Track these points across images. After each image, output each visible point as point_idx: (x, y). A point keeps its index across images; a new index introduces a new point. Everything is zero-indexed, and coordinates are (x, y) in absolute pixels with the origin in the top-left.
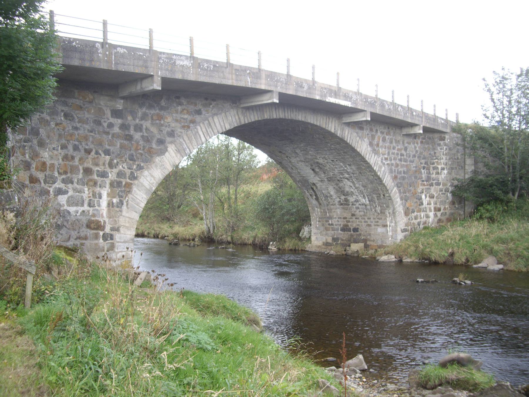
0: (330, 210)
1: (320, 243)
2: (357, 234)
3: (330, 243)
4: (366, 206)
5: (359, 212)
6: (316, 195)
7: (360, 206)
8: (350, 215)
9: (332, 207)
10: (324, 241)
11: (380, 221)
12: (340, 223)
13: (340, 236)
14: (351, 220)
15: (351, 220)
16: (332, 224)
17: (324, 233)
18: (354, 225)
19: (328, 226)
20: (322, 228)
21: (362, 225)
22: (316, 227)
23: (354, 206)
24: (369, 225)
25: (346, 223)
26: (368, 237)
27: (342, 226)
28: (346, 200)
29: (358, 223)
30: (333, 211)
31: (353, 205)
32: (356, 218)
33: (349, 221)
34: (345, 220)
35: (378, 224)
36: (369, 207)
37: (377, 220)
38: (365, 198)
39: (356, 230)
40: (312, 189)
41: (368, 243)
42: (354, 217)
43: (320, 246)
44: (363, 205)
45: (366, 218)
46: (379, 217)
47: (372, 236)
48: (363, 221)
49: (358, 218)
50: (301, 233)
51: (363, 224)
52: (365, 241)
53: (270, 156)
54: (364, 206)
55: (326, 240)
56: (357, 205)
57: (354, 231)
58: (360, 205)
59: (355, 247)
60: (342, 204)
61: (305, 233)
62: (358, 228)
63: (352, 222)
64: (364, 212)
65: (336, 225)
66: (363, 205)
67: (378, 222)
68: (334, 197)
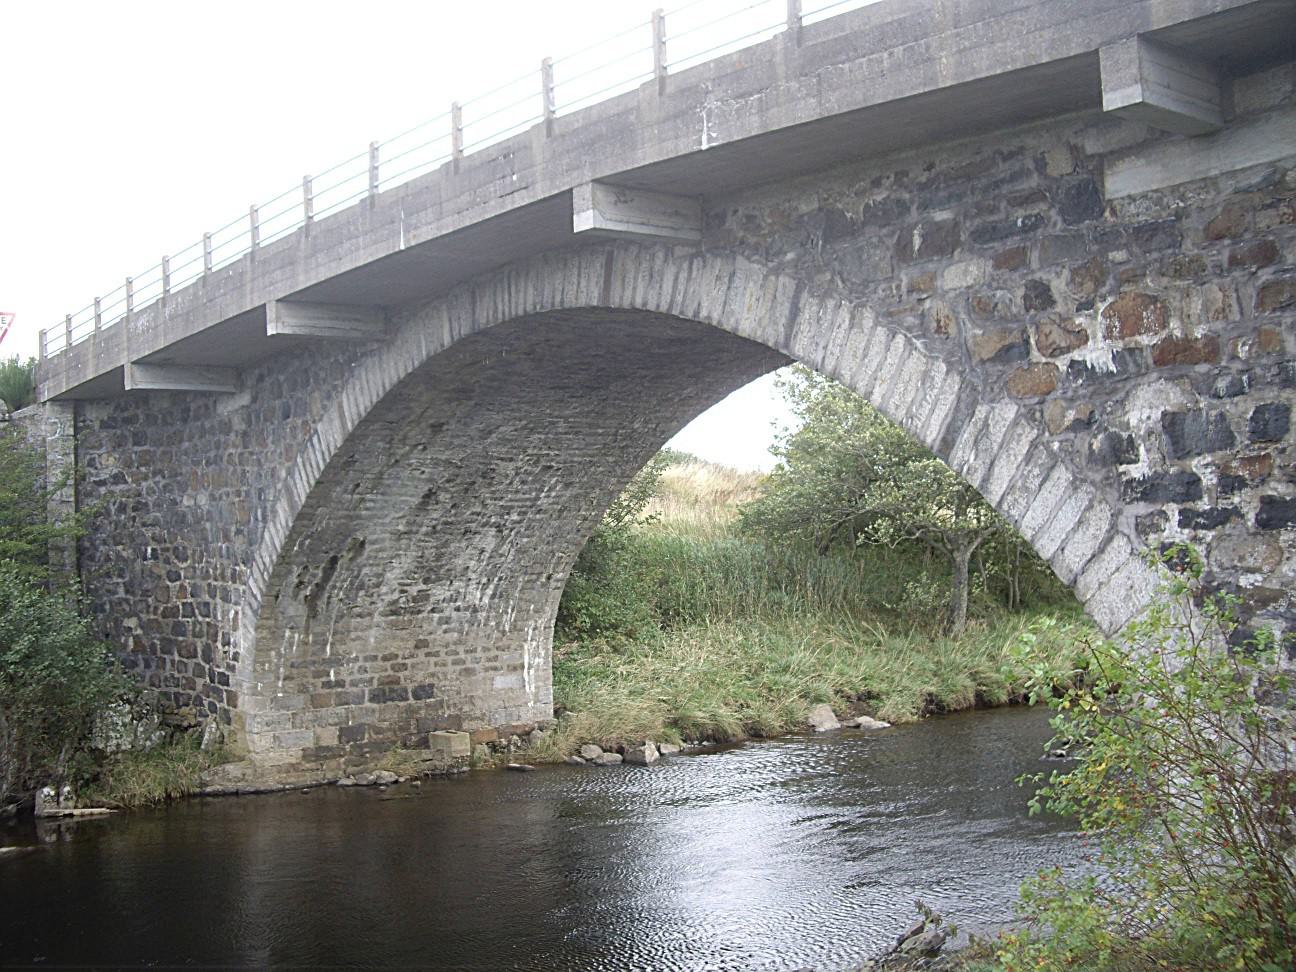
0: (341, 635)
1: (292, 755)
2: (428, 706)
3: (328, 748)
5: (445, 632)
7: (454, 614)
8: (411, 644)
9: (354, 622)
10: (310, 744)
11: (505, 656)
12: (367, 676)
16: (340, 683)
17: (309, 716)
18: (420, 677)
20: (299, 701)
21: (445, 674)
22: (274, 700)
24: (469, 672)
26: (466, 708)
27: (375, 682)
28: (423, 596)
29: (432, 669)
32: (428, 655)
34: (388, 664)
36: (482, 615)
39: (424, 691)
42: (421, 653)
44: (466, 609)
47: (478, 703)
49: (437, 654)
51: (450, 668)
55: (318, 738)
57: (417, 697)
58: (458, 609)
60: (394, 613)
62: (432, 686)
64: (461, 632)
65: (354, 684)
67: (496, 658)
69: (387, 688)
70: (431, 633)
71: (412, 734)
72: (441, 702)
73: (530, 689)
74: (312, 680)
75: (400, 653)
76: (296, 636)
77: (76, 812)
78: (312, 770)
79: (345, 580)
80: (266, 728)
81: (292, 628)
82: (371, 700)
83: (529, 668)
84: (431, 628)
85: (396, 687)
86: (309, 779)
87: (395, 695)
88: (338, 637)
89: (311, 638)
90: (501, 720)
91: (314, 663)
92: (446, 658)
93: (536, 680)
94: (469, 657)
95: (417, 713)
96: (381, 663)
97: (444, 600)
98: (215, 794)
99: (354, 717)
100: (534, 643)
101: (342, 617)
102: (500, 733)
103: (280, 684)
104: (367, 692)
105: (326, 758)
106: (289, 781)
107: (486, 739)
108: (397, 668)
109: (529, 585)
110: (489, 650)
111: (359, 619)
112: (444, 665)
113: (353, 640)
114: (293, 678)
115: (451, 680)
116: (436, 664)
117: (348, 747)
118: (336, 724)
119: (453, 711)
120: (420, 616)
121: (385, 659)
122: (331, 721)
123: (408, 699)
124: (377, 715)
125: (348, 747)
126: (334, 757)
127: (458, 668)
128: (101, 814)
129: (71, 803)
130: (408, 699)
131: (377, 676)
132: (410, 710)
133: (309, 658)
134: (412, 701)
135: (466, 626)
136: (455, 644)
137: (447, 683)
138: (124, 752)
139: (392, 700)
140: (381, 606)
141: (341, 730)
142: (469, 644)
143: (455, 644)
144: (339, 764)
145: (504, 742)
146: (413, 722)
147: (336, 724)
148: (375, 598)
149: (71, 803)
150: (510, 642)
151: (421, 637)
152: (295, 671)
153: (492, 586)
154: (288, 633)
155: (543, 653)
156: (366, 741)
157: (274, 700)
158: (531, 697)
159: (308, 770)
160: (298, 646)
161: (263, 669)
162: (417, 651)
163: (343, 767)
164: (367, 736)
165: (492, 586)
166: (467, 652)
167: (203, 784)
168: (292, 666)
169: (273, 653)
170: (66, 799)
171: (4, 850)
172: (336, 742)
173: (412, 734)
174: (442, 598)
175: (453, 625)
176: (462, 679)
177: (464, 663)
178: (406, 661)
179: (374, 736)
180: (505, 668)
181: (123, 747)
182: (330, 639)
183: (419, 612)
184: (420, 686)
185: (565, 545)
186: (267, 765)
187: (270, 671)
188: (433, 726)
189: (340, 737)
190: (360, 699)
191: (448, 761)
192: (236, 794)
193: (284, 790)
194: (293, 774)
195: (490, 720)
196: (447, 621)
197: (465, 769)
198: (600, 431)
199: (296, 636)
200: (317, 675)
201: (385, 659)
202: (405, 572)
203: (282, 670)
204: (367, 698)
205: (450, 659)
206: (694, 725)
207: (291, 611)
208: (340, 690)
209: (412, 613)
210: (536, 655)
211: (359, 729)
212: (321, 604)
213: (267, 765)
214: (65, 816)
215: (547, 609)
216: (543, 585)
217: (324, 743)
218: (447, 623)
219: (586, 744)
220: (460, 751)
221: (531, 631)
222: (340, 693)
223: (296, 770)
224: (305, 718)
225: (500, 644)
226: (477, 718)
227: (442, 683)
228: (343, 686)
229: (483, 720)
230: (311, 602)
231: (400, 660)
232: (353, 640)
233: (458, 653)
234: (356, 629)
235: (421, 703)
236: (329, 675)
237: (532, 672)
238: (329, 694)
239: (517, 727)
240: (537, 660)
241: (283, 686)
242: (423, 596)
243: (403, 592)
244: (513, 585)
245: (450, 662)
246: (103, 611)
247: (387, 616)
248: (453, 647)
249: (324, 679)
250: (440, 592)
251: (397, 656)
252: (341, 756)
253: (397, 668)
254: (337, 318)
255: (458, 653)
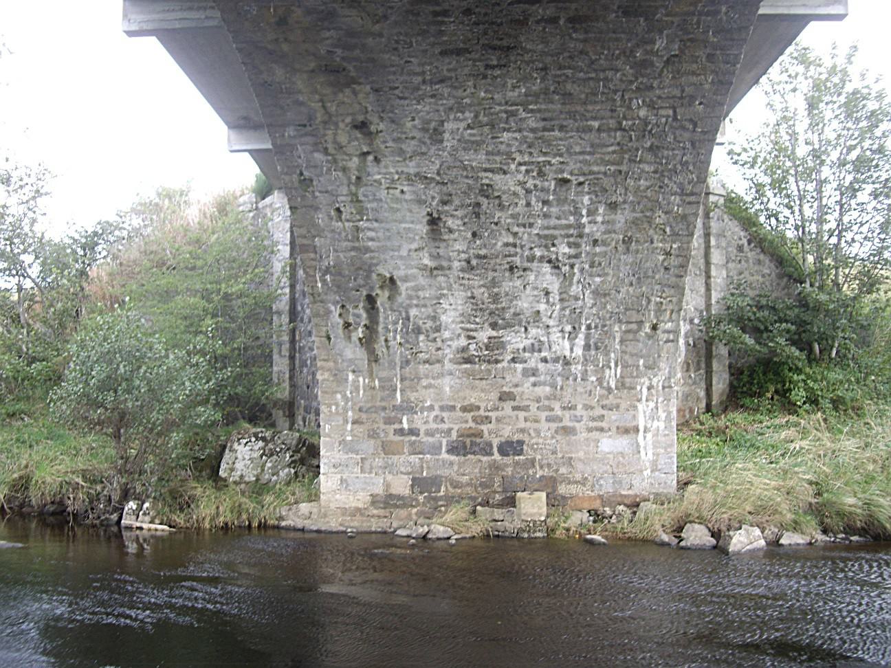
0: (412, 382)
1: (360, 499)
2: (517, 463)
3: (399, 497)
4: (567, 363)
5: (534, 385)
6: (371, 329)
7: (541, 366)
8: (494, 396)
9: (423, 369)
10: (379, 490)
11: (613, 416)
12: (445, 426)
13: (445, 472)
14: (493, 415)
15: (493, 415)
16: (413, 432)
17: (378, 462)
18: (507, 432)
19: (392, 437)
20: (369, 446)
21: (538, 432)
22: (342, 442)
23: (519, 367)
24: (567, 431)
25: (471, 424)
26: (563, 470)
27: (454, 435)
28: (495, 345)
29: (522, 425)
30: (424, 382)
31: (513, 360)
32: (514, 408)
33: (488, 420)
34: (469, 416)
35: (604, 424)
36: (577, 369)
37: (598, 411)
38: (572, 336)
39: (511, 448)
40: (371, 300)
41: (562, 489)
42: (508, 406)
43: (358, 510)
44: (556, 360)
45: (557, 406)
46: (611, 400)
47: (580, 466)
48: (543, 415)
49: (526, 409)
50: (223, 466)
51: (544, 425)
52: (549, 485)
53: (279, 171)
54: (559, 367)
55: (387, 485)
56: (532, 363)
57: (503, 451)
58: (545, 360)
59: (533, 506)
60: (468, 361)
61: (239, 465)
62: (521, 443)
63: (498, 420)
64: (554, 386)
65: (429, 433)
66: (556, 360)
67: (602, 418)
68: (447, 334)
69: (468, 441)
70: (517, 386)
71: (495, 492)
72: (533, 462)
73: (647, 456)
74: (382, 426)
75: (483, 405)
76: (361, 379)
77: (145, 526)
78: (379, 517)
79: (395, 323)
80: (333, 470)
81: (354, 371)
82: (448, 452)
83: (645, 432)
84: (515, 380)
85: (478, 440)
86: (375, 525)
87: (477, 449)
88: (407, 383)
89: (377, 382)
90: (607, 487)
91: (384, 409)
92: (539, 413)
93: (655, 447)
94: (567, 414)
95: (503, 470)
96: (461, 414)
97: (524, 350)
98: (287, 529)
99: (428, 468)
100: (652, 405)
101: (408, 362)
102: (605, 501)
103: (349, 427)
104: (444, 443)
105: (397, 506)
106: (352, 524)
107: (587, 505)
108: (480, 420)
109: (631, 336)
110: (592, 408)
111: (427, 366)
112: (536, 421)
113: (425, 387)
114: (362, 423)
115: (545, 438)
116: (526, 420)
117: (421, 498)
118: (409, 473)
119: (546, 472)
120: (499, 365)
121: (464, 409)
122: (403, 469)
123: (493, 455)
124: (456, 468)
125: (421, 498)
126: (404, 506)
127: (554, 425)
128: (163, 530)
129: (147, 518)
130: (493, 455)
131: (456, 427)
132: (495, 467)
133: (378, 404)
134: (497, 456)
135: (559, 379)
136: (548, 398)
137: (541, 441)
138: (247, 483)
139: (474, 453)
140: (449, 353)
141: (414, 479)
142: (566, 400)
143: (548, 398)
144: (410, 514)
145: (608, 511)
146: (497, 480)
147: (409, 473)
148: (439, 344)
149: (147, 518)
150: (619, 401)
151: (505, 389)
152: (364, 416)
153: (581, 336)
154: (351, 377)
155: (663, 415)
156: (442, 493)
157: (342, 442)
158: (648, 464)
159: (373, 516)
160: (364, 391)
161: (330, 411)
162: (502, 404)
163: (414, 517)
164: (443, 489)
165: (581, 336)
166: (564, 408)
167: (281, 518)
168: (360, 410)
169: (339, 396)
170: (145, 514)
171: (2, 542)
172: (407, 492)
173: (495, 492)
174: (521, 346)
175: (542, 378)
176: (559, 437)
177: (561, 420)
178: (490, 414)
179: (451, 489)
180: (614, 429)
181: (247, 479)
182: (399, 386)
183: (497, 362)
184: (507, 442)
185: (658, 287)
186: (333, 506)
187: (337, 413)
188: (522, 485)
189: (412, 486)
190: (436, 449)
191: (518, 524)
192: (303, 530)
193: (345, 532)
194: (358, 517)
195: (593, 486)
196: (534, 372)
197: (539, 534)
198: (596, 124)
199: (361, 379)
200: (389, 421)
201: (464, 409)
202: (462, 315)
203: (350, 413)
204: (444, 449)
205: (543, 415)
206: (838, 513)
207: (349, 354)
208: (414, 438)
209: (489, 362)
210: (654, 417)
211: (435, 482)
212: (380, 348)
213: (333, 506)
214: (137, 528)
215: (662, 365)
216: (649, 337)
217: (394, 491)
218: (534, 375)
219: (691, 522)
220: (531, 515)
221: (645, 391)
222: (414, 442)
223: (362, 515)
224: (374, 464)
225: (604, 402)
226: (576, 482)
227: (534, 441)
228: (418, 435)
229: (584, 485)
230: (368, 342)
231: (482, 412)
232: (425, 387)
233: (553, 410)
234: (427, 377)
235: (508, 460)
236: (401, 422)
237: (649, 436)
238: (403, 441)
239: (625, 496)
240: (656, 423)
241: (352, 431)
242: (495, 345)
243: (469, 337)
244: (608, 334)
245: (544, 418)
246: (306, 366)
247: (460, 363)
248: (547, 403)
249: (397, 426)
250: (516, 340)
251: (478, 408)
252: (413, 506)
253: (480, 420)
254: (190, 9)
255: (553, 410)
